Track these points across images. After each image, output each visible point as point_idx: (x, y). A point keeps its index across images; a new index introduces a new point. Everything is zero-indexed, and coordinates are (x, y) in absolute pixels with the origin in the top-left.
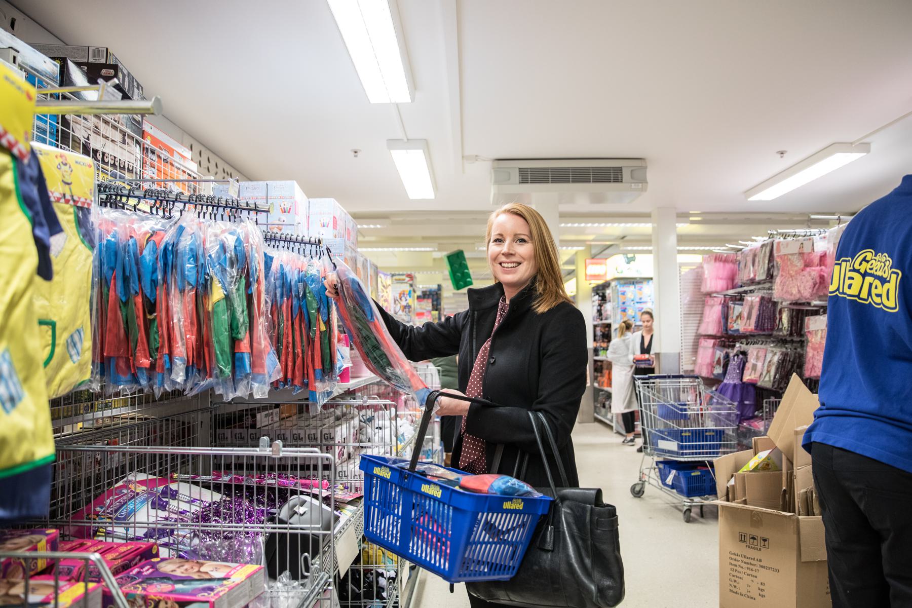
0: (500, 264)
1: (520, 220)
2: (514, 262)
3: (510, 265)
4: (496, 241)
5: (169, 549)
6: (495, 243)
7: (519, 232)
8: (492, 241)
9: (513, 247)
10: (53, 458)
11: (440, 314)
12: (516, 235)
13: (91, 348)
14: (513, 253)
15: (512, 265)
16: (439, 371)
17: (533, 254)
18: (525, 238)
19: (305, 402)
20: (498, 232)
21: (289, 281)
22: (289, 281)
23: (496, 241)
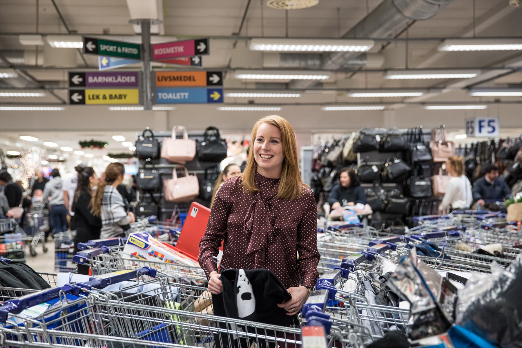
0: (260, 155)
1: (275, 129)
2: (268, 155)
3: (266, 157)
4: (259, 140)
5: (102, 204)
6: (258, 141)
7: (274, 136)
8: (256, 139)
9: (269, 145)
10: (192, 159)
11: (463, 241)
12: (271, 138)
13: (75, 189)
14: (269, 149)
15: (268, 157)
16: (163, 241)
17: (281, 150)
18: (278, 140)
19: (109, 202)
20: (260, 135)
21: (238, 286)
22: (238, 286)
23: (259, 140)
